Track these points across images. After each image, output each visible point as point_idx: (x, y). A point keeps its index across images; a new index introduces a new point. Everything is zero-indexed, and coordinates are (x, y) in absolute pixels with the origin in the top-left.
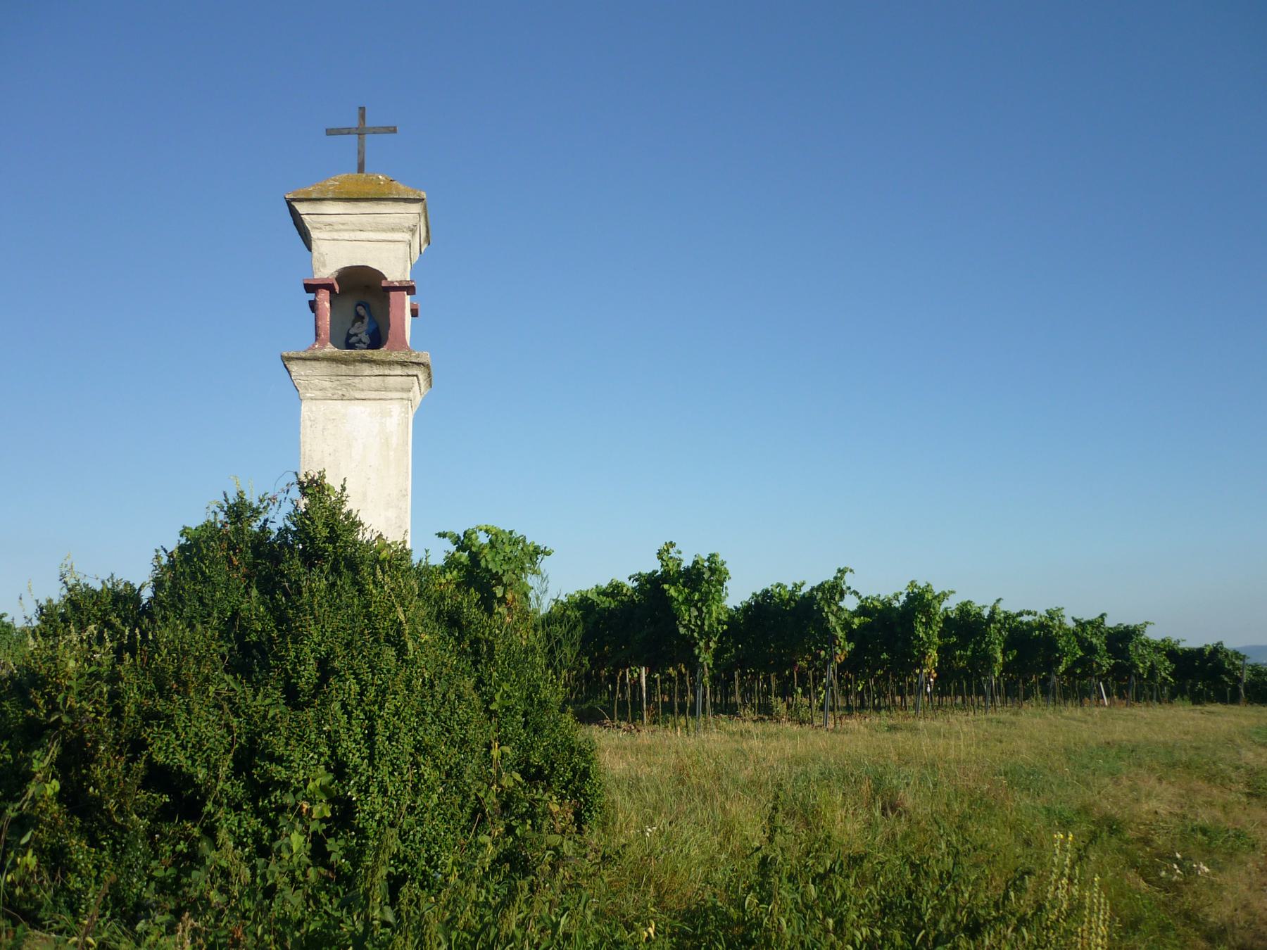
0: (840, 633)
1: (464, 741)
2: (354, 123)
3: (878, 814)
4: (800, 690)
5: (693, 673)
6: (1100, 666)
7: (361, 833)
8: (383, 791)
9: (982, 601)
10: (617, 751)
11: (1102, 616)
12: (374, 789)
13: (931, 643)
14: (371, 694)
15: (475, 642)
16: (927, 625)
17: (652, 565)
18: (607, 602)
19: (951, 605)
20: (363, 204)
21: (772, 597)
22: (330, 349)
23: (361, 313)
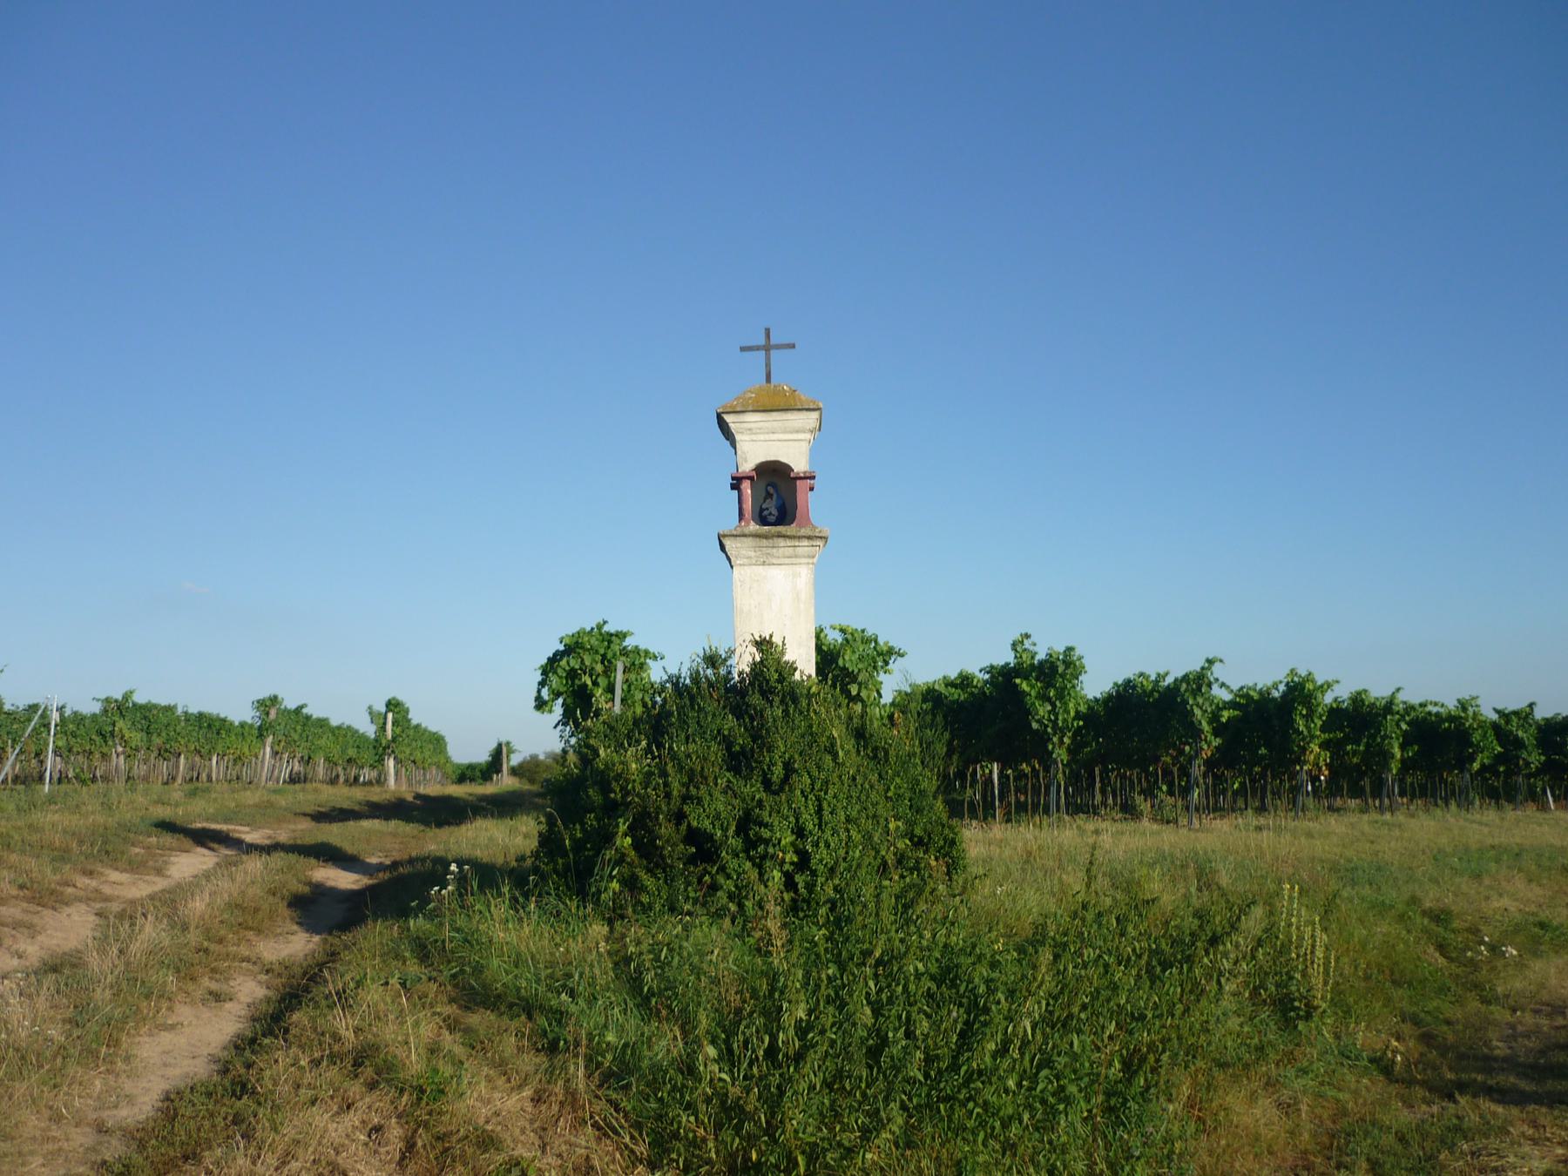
0: (1205, 726)
1: (875, 816)
2: (762, 341)
3: (1193, 890)
4: (1164, 788)
5: (1047, 770)
6: (1528, 764)
7: (814, 873)
8: (828, 846)
9: (1378, 691)
10: (975, 839)
11: (1531, 705)
12: (822, 845)
13: (1313, 737)
14: (818, 786)
15: (875, 749)
16: (1309, 717)
17: (1006, 657)
18: (955, 694)
19: (1341, 693)
20: (774, 414)
21: (1134, 687)
22: (753, 527)
23: (775, 499)
